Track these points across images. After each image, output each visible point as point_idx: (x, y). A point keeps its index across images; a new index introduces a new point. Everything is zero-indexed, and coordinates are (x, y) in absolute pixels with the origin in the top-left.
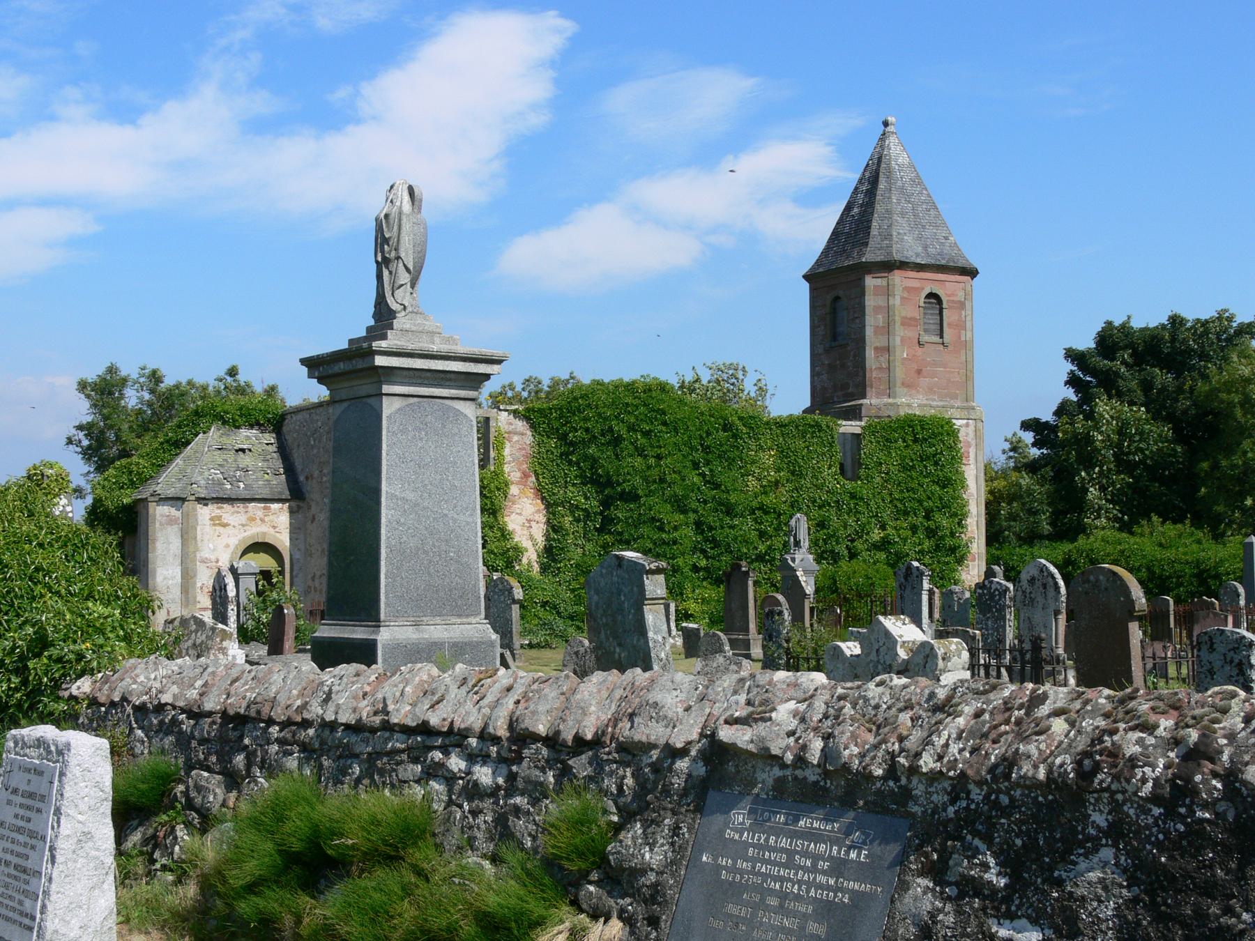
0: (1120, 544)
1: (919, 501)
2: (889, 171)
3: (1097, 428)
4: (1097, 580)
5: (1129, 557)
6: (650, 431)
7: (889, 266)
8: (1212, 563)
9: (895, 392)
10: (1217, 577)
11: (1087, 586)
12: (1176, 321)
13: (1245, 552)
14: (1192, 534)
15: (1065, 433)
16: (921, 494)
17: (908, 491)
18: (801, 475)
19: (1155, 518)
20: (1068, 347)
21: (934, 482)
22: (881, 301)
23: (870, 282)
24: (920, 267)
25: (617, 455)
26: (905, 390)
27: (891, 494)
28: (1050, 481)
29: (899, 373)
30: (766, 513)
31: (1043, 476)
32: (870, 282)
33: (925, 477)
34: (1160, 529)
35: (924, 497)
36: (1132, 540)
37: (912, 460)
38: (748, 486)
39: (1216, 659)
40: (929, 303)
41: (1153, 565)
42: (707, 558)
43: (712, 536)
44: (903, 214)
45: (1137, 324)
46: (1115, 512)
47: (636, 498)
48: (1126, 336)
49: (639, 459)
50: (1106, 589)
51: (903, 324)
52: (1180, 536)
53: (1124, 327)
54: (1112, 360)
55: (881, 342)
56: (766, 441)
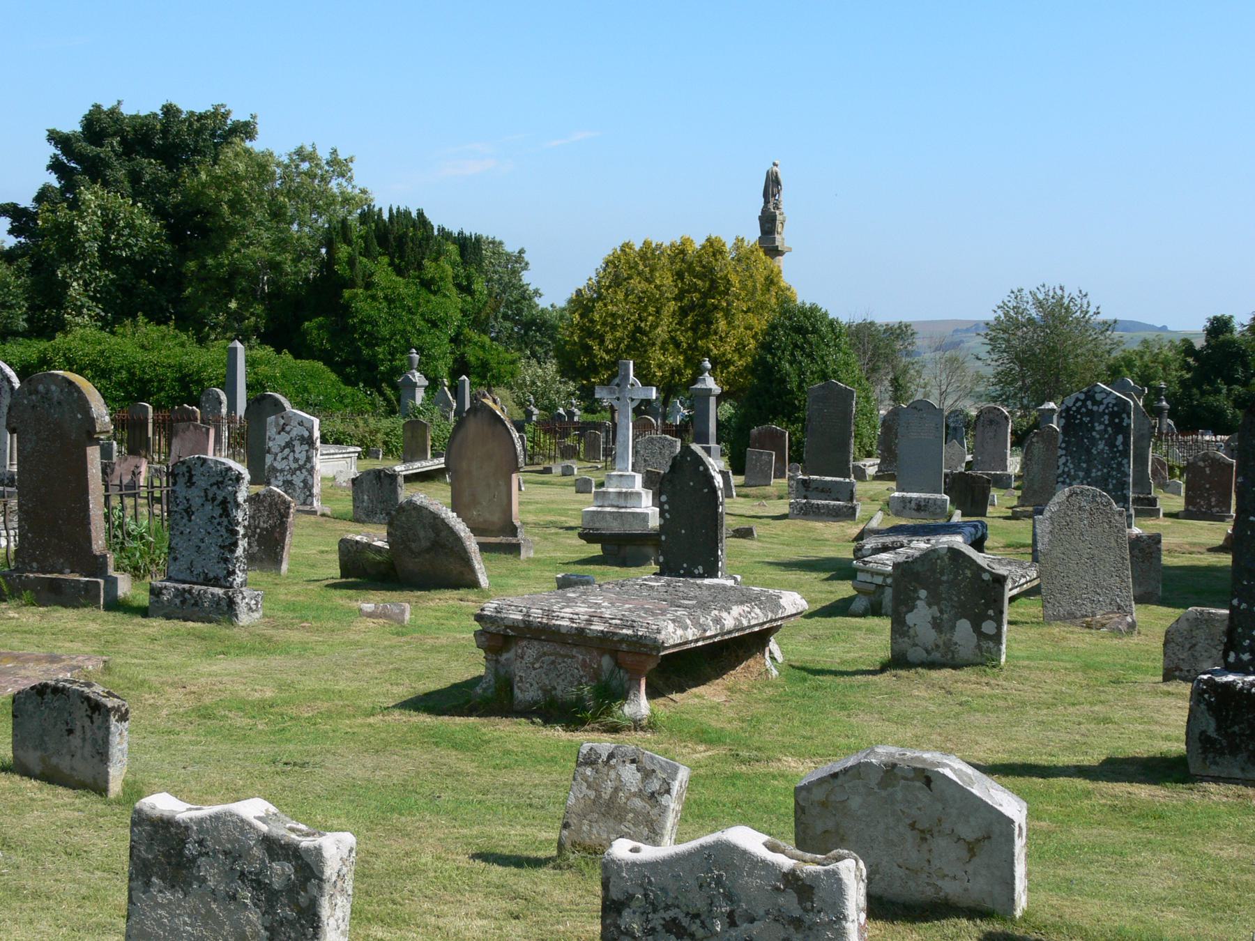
0: (100, 344)
3: (81, 217)
4: (48, 391)
5: (109, 357)
8: (194, 367)
10: (199, 382)
11: (34, 397)
12: (169, 111)
13: (228, 357)
14: (176, 337)
15: (45, 221)
28: (27, 273)
31: (19, 268)
34: (144, 329)
36: (113, 340)
39: (195, 495)
41: (134, 367)
45: (127, 110)
46: (98, 310)
48: (115, 122)
50: (59, 403)
52: (163, 338)
53: (113, 112)
54: (101, 146)
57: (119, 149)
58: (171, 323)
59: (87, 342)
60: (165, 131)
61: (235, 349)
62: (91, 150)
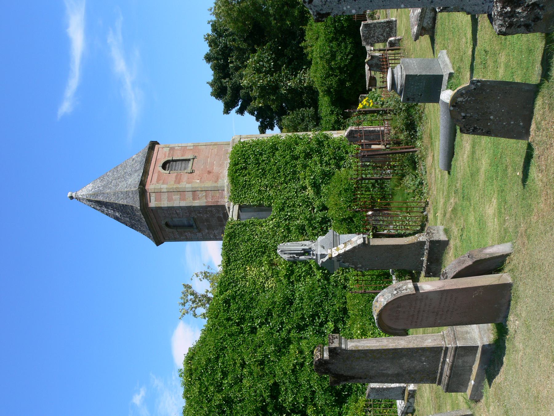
1: (286, 164)
2: (96, 195)
6: (222, 372)
7: (143, 192)
9: (221, 187)
12: (208, 58)
16: (281, 163)
17: (279, 172)
18: (266, 247)
19: (303, 44)
20: (223, 113)
21: (273, 155)
22: (165, 196)
23: (153, 204)
24: (146, 173)
25: (240, 401)
26: (220, 180)
27: (282, 184)
29: (209, 184)
30: (292, 272)
32: (153, 204)
33: (270, 161)
35: (283, 161)
37: (258, 170)
38: (272, 287)
40: (169, 168)
42: (327, 321)
43: (309, 317)
44: (116, 185)
47: (276, 384)
49: (244, 381)
51: (179, 183)
55: (189, 195)
56: (238, 273)
57: (227, 79)
58: (304, 27)
59: (316, 70)
60: (217, 59)
61: (372, 389)
62: (229, 91)
